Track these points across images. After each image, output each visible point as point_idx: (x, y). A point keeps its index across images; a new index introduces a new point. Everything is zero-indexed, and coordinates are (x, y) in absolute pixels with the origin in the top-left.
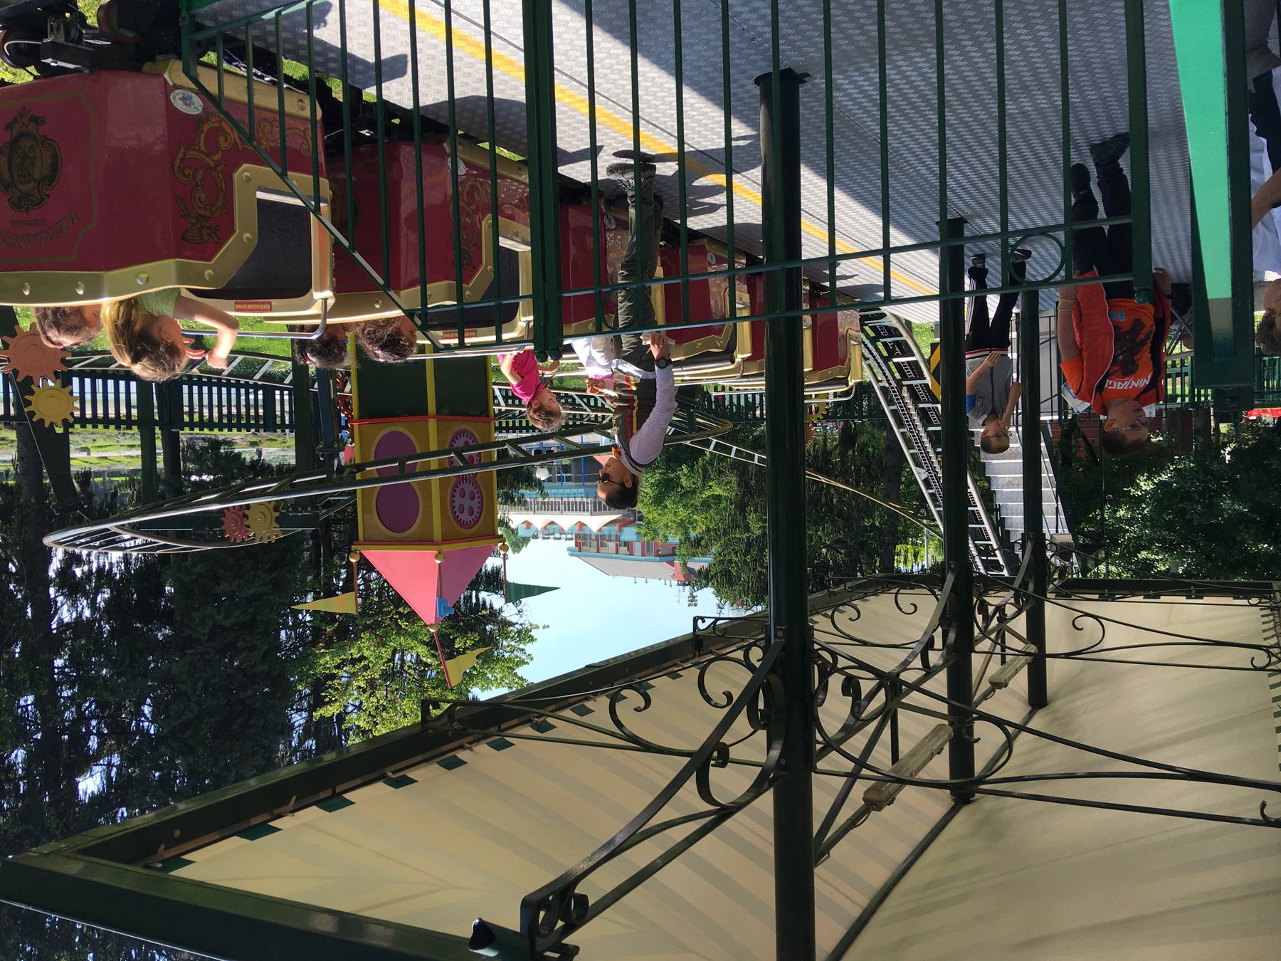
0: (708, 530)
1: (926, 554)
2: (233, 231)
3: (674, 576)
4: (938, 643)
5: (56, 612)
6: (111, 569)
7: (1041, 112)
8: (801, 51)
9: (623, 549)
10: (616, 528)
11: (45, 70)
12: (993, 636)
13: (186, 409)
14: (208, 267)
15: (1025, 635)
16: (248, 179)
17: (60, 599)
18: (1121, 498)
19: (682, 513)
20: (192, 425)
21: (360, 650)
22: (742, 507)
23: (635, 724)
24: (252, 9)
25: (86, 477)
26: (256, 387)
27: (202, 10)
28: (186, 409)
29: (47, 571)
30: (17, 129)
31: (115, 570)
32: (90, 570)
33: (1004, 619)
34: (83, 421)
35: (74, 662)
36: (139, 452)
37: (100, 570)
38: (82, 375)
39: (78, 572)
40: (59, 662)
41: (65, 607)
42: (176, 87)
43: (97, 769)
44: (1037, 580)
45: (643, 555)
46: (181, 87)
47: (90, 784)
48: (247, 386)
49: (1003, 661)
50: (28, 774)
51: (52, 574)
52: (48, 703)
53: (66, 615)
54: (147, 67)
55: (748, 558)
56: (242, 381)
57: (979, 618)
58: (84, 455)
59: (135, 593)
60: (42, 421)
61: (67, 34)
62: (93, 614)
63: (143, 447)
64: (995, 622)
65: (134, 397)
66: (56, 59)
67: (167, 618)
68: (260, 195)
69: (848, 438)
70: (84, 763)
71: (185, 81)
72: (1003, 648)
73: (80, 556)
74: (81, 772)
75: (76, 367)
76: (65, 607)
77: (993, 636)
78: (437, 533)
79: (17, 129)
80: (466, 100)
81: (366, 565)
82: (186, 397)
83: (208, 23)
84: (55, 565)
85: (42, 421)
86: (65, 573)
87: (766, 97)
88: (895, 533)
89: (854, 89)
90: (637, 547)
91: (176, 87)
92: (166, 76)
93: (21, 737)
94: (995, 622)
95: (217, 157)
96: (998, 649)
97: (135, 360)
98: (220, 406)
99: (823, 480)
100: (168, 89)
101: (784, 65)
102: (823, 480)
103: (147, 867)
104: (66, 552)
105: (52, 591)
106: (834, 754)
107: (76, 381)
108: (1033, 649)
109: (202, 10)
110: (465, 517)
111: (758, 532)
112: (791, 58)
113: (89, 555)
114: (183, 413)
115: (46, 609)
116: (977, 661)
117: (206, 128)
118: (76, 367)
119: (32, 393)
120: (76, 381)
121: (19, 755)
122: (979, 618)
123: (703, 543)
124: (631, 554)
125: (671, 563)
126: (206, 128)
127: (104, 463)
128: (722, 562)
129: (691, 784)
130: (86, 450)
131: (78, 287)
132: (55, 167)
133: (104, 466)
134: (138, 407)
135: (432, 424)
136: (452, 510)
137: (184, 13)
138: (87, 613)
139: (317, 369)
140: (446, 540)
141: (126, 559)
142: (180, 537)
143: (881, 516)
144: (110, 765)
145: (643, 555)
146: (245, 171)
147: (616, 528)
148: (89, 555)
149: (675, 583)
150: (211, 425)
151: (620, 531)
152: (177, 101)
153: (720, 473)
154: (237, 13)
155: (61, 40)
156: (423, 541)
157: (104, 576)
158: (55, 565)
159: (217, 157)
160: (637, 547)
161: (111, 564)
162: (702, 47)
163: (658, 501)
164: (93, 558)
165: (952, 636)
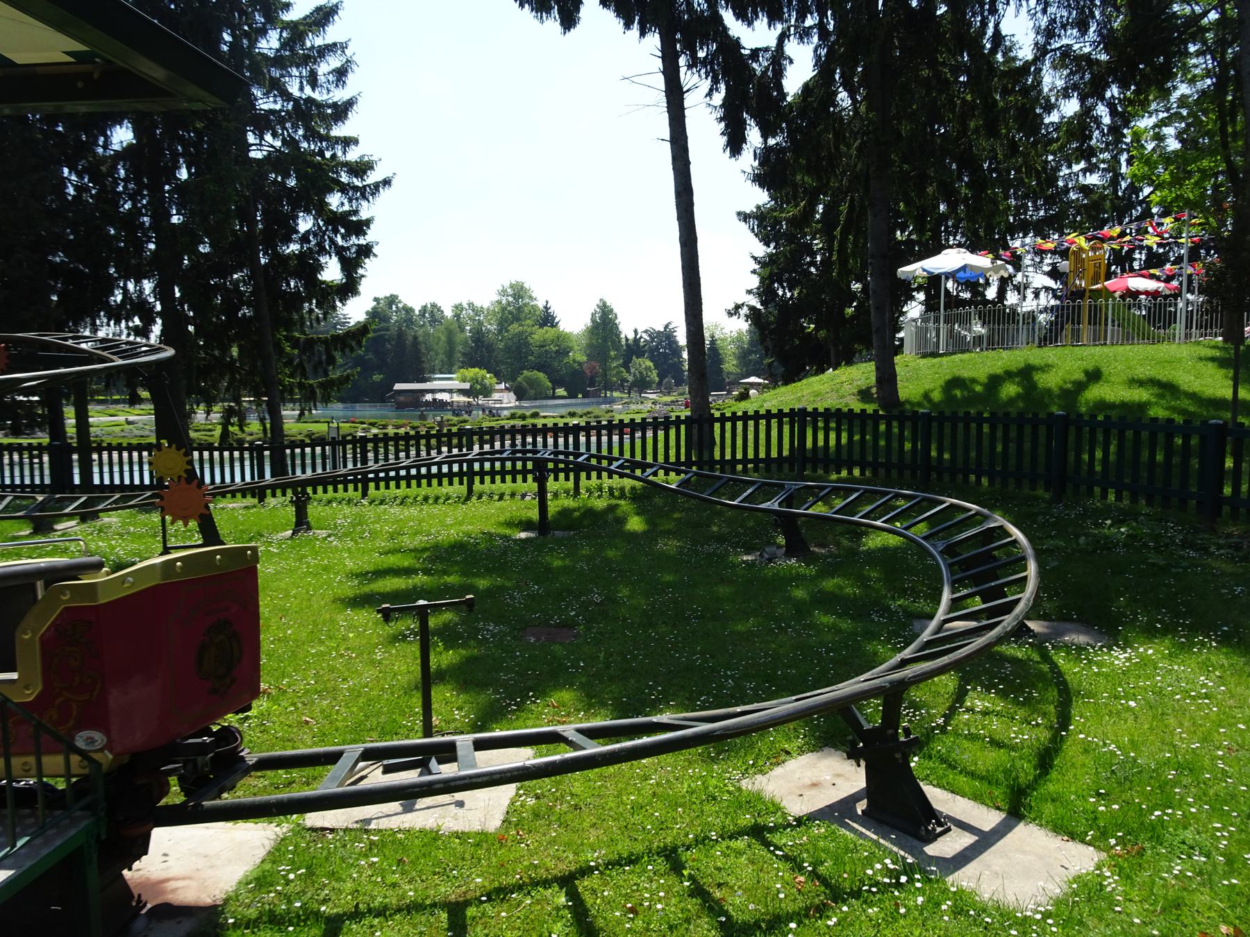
2: (44, 642)
5: (155, 288)
6: (109, 320)
11: (209, 733)
14: (67, 602)
16: (27, 688)
17: (152, 300)
20: (40, 447)
24: (37, 841)
25: (134, 400)
27: (85, 823)
29: (163, 324)
31: (105, 320)
32: (127, 321)
34: (149, 447)
35: (141, 248)
37: (118, 322)
38: (142, 487)
39: (137, 321)
40: (152, 246)
41: (147, 292)
42: (101, 750)
43: (116, 147)
46: (96, 751)
47: (122, 136)
50: (175, 156)
51: (159, 321)
52: (161, 216)
53: (148, 286)
54: (126, 759)
58: (131, 418)
59: (89, 301)
60: (178, 449)
61: (195, 764)
62: (125, 285)
63: (88, 425)
65: (96, 469)
66: (204, 743)
67: (56, 270)
68: (15, 676)
69: (1006, 247)
70: (127, 153)
71: (96, 756)
73: (136, 335)
74: (130, 146)
75: (149, 494)
82: (47, 472)
83: (78, 814)
84: (157, 329)
85: (178, 449)
86: (148, 320)
91: (101, 750)
92: (111, 756)
93: (181, 187)
95: (60, 699)
98: (21, 464)
100: (109, 746)
103: (110, 62)
104: (148, 338)
105: (159, 308)
107: (147, 482)
109: (85, 823)
113: (129, 335)
115: (163, 292)
117: (71, 723)
118: (149, 494)
120: (147, 482)
121: (183, 174)
126: (71, 723)
127: (112, 412)
130: (129, 423)
131: (181, 567)
133: (113, 408)
134: (71, 461)
137: (102, 814)
138: (131, 286)
139: (447, 648)
141: (95, 330)
142: (47, 346)
144: (105, 147)
146: (30, 695)
148: (129, 335)
150: (20, 449)
152: (99, 737)
154: (51, 832)
155: (200, 759)
157: (116, 314)
158: (157, 329)
159: (60, 699)
161: (108, 325)
164: (125, 332)
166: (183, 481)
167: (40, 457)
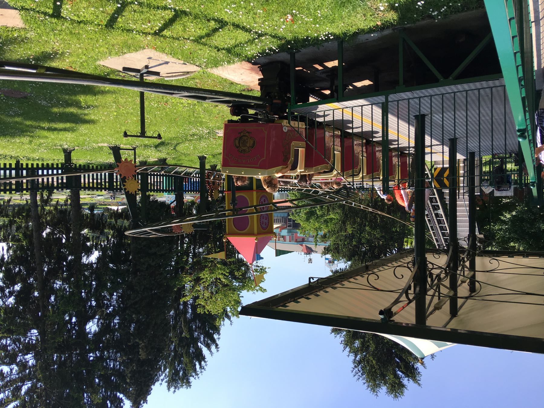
0: (329, 232)
1: (409, 244)
3: (302, 251)
4: (411, 291)
7: (487, 120)
8: (425, 110)
9: (282, 239)
10: (279, 230)
12: (435, 288)
13: (115, 180)
15: (449, 286)
18: (498, 221)
19: (317, 225)
21: (204, 275)
22: (344, 223)
23: (378, 284)
25: (92, 207)
26: (163, 175)
28: (115, 180)
30: (242, 134)
33: (440, 279)
36: (81, 197)
44: (474, 251)
45: (290, 241)
48: (160, 175)
49: (439, 299)
55: (346, 243)
56: (152, 173)
57: (429, 280)
60: (128, 191)
64: (436, 282)
72: (439, 293)
76: (85, 257)
77: (435, 288)
78: (256, 231)
79: (242, 134)
80: (337, 120)
81: (229, 242)
85: (128, 191)
87: (418, 122)
88: (404, 233)
89: (437, 118)
90: (288, 238)
94: (436, 282)
96: (437, 294)
97: (268, 187)
99: (379, 213)
101: (422, 113)
102: (379, 213)
106: (432, 294)
108: (452, 293)
110: (264, 226)
111: (350, 232)
112: (423, 111)
114: (114, 182)
116: (428, 298)
119: (126, 182)
122: (429, 280)
123: (327, 236)
124: (285, 241)
125: (302, 245)
128: (335, 244)
129: (404, 295)
132: (254, 144)
135: (255, 193)
136: (260, 223)
140: (259, 234)
143: (400, 227)
145: (290, 241)
147: (279, 230)
149: (303, 253)
151: (281, 231)
153: (333, 209)
156: (251, 234)
160: (288, 238)
162: (404, 111)
163: (308, 220)
165: (418, 289)
166: (127, 177)
167: (157, 188)
